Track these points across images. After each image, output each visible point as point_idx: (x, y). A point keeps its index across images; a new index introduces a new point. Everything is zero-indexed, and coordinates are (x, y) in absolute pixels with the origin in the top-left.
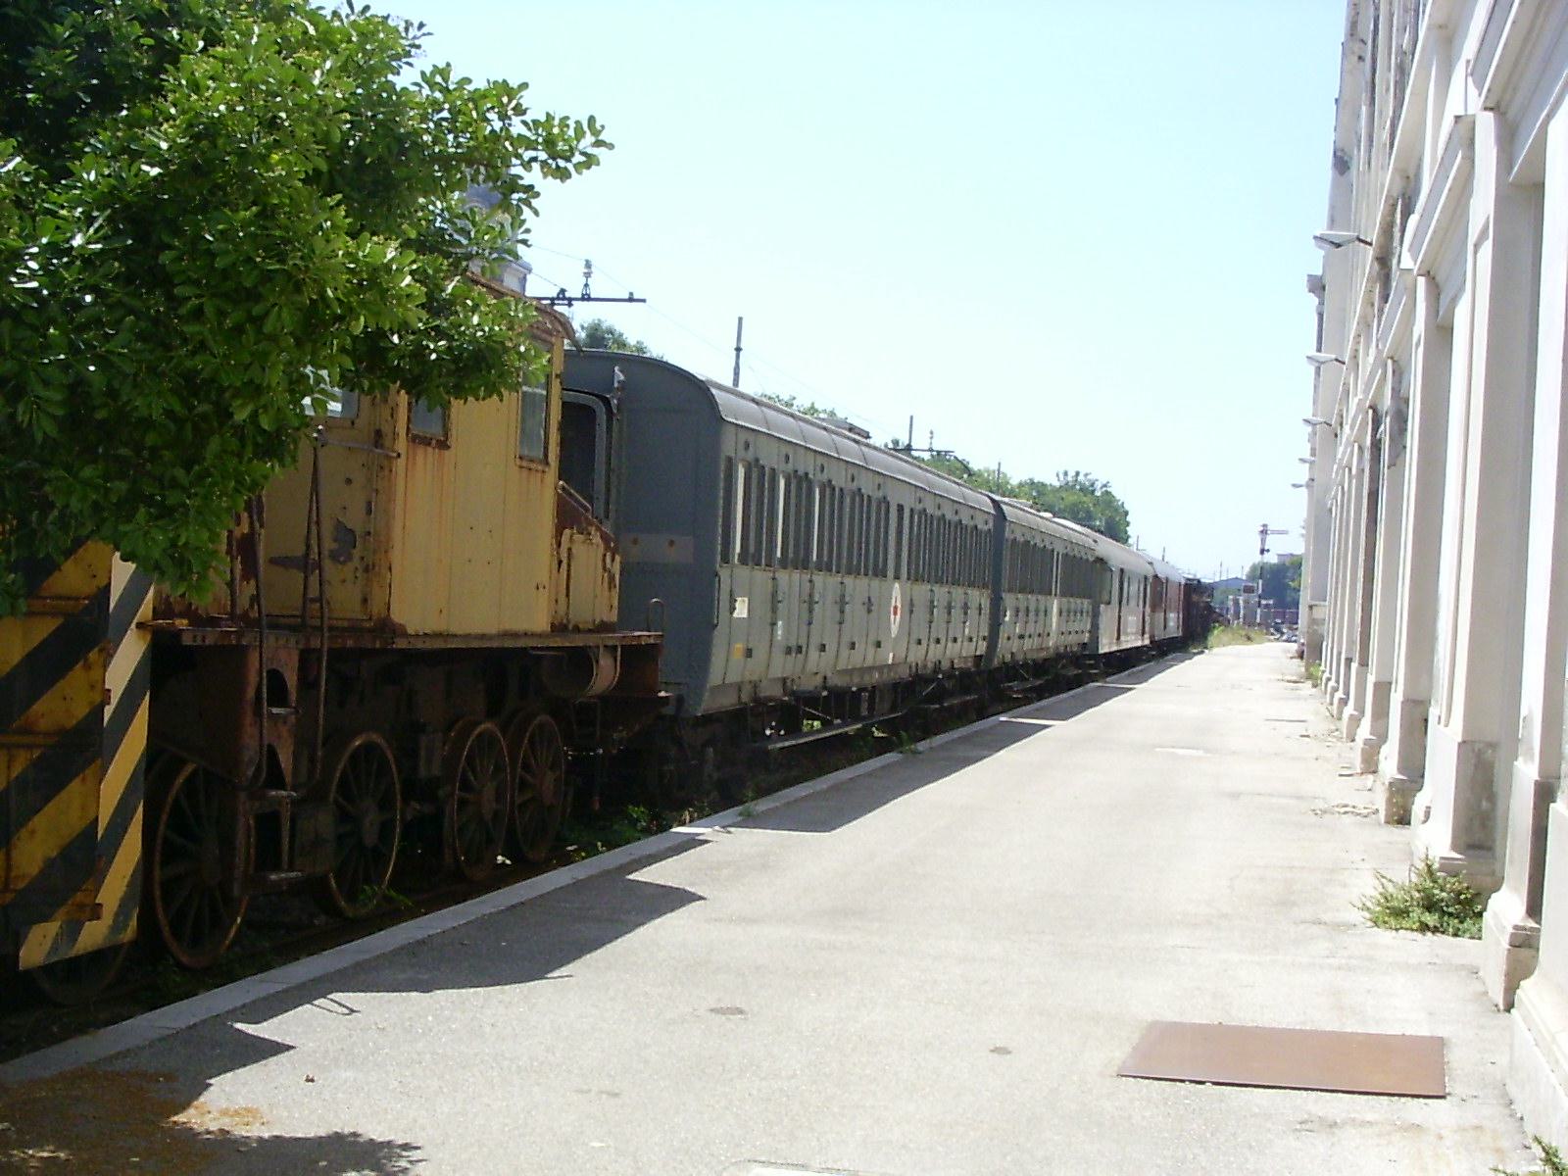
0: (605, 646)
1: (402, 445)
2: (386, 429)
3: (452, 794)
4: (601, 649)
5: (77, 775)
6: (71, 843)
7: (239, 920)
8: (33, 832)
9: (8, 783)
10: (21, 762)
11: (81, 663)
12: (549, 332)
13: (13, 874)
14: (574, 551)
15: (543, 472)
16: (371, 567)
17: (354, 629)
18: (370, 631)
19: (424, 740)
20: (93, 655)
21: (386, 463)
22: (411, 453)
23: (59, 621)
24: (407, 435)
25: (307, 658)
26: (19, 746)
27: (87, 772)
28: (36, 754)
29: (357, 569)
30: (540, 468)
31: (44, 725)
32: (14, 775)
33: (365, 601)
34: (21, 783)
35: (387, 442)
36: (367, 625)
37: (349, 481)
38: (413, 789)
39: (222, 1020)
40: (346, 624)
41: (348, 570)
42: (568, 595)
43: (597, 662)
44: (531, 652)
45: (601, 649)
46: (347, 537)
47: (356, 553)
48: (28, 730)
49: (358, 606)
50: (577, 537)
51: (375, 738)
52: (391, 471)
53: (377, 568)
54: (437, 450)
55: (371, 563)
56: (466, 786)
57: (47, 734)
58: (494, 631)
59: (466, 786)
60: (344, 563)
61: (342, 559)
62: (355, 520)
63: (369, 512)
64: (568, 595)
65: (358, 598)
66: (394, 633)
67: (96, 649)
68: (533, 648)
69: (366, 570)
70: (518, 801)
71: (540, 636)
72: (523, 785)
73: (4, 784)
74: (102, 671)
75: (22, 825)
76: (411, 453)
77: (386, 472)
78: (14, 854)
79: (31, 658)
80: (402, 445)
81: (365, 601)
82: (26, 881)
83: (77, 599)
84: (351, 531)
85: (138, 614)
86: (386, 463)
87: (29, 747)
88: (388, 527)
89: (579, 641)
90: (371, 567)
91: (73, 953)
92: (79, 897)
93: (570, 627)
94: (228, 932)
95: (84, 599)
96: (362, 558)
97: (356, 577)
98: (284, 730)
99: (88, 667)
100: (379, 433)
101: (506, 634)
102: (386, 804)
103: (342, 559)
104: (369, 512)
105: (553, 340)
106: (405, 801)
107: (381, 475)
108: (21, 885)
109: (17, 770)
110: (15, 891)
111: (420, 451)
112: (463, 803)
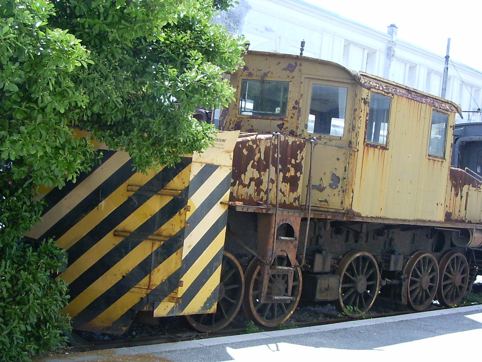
0: (476, 229)
1: (361, 147)
2: (353, 140)
3: (408, 278)
4: (474, 230)
5: (175, 252)
6: (171, 276)
7: (292, 312)
8: (159, 270)
9: (152, 252)
10: (157, 245)
11: (178, 213)
12: (447, 110)
13: (151, 283)
14: (469, 193)
15: (442, 162)
16: (345, 191)
17: (336, 212)
18: (343, 213)
19: (393, 257)
20: (182, 210)
21: (353, 153)
22: (366, 150)
23: (172, 198)
24: (364, 143)
25: (304, 220)
26: (156, 240)
27: (178, 251)
28: (162, 243)
29: (340, 191)
30: (440, 160)
31: (165, 233)
32: (154, 250)
33: (342, 203)
34: (157, 252)
35: (354, 145)
36: (342, 211)
37: (338, 159)
38: (386, 274)
39: (224, 346)
40: (334, 211)
41: (336, 191)
42: (466, 209)
43: (472, 234)
44: (436, 228)
45: (474, 230)
46: (336, 180)
47: (340, 186)
48: (159, 235)
49: (340, 205)
50: (471, 188)
51: (367, 254)
52: (355, 156)
53: (347, 191)
54: (381, 150)
55: (345, 189)
56: (415, 275)
57: (165, 237)
58: (413, 219)
59: (415, 275)
60: (335, 188)
61: (334, 187)
62: (340, 173)
63: (345, 170)
64: (466, 209)
65: (340, 202)
66: (354, 215)
67: (183, 209)
68: (436, 227)
69: (343, 191)
70: (443, 284)
71: (439, 222)
72: (447, 278)
73: (151, 253)
74: (185, 216)
75: (155, 267)
76: (366, 150)
77: (353, 157)
78: (152, 277)
79: (162, 210)
80: (361, 147)
81: (342, 203)
82: (155, 287)
83: (176, 190)
84: (338, 177)
85: (221, 199)
86: (353, 153)
87: (160, 241)
88: (353, 178)
89: (468, 226)
90: (345, 191)
91: (182, 314)
92: (172, 294)
93: (467, 221)
94: (286, 316)
95: (180, 190)
96: (342, 187)
97: (339, 194)
98: (292, 246)
99: (180, 214)
100: (350, 142)
101: (418, 220)
102: (372, 278)
103: (334, 187)
104: (345, 170)
105: (449, 113)
106: (383, 278)
107: (351, 157)
108: (153, 288)
109: (155, 248)
110: (151, 289)
111: (371, 150)
112: (413, 283)
